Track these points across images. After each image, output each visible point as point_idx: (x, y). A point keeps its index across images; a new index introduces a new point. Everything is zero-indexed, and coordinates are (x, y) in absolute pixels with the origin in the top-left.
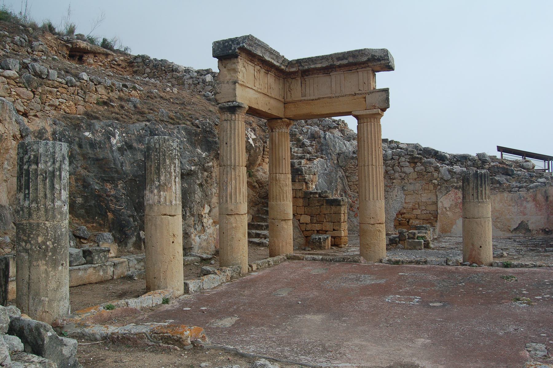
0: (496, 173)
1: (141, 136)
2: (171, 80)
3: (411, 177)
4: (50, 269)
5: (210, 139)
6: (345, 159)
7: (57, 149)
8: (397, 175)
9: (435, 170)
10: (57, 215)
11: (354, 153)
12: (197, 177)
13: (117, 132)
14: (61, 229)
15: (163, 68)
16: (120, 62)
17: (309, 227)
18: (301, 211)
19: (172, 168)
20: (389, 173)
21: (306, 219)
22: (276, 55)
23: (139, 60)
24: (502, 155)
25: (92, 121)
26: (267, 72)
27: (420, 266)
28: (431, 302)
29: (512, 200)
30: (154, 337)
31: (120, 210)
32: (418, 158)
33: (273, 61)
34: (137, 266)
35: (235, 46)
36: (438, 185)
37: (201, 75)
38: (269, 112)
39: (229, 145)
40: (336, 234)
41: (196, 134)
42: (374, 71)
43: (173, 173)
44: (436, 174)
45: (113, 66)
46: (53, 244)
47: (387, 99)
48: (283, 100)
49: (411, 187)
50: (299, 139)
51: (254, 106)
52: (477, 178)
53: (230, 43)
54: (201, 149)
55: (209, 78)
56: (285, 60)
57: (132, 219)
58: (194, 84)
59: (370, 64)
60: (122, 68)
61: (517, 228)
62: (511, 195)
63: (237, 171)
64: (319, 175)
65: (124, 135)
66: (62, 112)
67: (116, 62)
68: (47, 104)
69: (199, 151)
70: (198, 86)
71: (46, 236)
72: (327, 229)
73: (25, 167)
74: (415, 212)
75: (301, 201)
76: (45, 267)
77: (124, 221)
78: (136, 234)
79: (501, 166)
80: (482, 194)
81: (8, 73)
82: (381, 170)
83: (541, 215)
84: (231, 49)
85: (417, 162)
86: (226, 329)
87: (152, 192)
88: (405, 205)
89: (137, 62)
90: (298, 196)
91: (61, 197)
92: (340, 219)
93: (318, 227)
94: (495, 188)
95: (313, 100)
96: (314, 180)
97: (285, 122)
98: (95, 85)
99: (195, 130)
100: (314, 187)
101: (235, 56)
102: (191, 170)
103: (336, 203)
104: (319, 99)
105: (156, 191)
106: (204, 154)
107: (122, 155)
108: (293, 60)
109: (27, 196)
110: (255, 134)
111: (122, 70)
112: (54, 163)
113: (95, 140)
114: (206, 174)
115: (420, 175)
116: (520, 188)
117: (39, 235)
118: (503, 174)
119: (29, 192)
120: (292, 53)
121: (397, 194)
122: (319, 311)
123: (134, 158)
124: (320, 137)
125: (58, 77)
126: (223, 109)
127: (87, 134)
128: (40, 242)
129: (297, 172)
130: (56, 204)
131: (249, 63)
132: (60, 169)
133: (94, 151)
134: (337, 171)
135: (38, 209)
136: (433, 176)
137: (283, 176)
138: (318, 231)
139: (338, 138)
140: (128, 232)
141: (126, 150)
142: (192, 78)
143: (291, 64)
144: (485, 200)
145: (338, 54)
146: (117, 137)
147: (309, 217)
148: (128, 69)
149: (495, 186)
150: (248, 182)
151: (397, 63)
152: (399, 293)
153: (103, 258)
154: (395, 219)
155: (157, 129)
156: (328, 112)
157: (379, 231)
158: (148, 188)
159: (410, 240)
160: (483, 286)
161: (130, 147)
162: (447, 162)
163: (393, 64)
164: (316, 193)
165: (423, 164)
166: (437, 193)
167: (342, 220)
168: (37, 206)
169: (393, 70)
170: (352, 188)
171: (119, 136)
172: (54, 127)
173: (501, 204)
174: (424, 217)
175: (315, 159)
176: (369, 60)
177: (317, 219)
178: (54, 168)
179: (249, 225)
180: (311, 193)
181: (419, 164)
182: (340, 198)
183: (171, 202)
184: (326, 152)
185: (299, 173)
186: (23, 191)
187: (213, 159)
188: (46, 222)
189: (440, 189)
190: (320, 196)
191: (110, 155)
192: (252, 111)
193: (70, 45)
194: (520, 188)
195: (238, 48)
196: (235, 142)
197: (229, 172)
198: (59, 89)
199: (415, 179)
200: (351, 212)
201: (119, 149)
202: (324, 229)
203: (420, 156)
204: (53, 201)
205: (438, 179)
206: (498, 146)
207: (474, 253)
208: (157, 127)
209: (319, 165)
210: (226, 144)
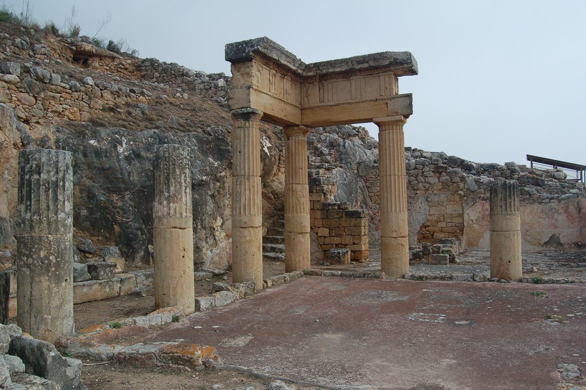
1: (149, 144)
3: (435, 187)
5: (223, 148)
6: (365, 168)
7: (61, 158)
8: (420, 185)
9: (461, 181)
11: (375, 162)
14: (65, 242)
15: (173, 72)
16: (128, 66)
17: (327, 241)
19: (183, 178)
20: (412, 183)
21: (324, 232)
22: (288, 55)
23: (148, 64)
24: (532, 164)
26: (283, 76)
27: (445, 282)
28: (457, 320)
29: (542, 212)
30: (164, 357)
31: (127, 223)
32: (443, 167)
35: (249, 48)
36: (464, 196)
37: (213, 79)
38: (285, 118)
39: (242, 153)
40: (356, 247)
42: (396, 76)
43: (184, 184)
44: (462, 185)
45: (120, 70)
47: (411, 105)
48: (300, 106)
49: (436, 199)
51: (270, 112)
54: (214, 158)
55: (221, 83)
56: (302, 64)
58: (206, 89)
59: (392, 68)
60: (129, 72)
62: (541, 206)
63: (251, 181)
64: (338, 186)
65: (131, 143)
66: (66, 119)
67: (123, 65)
68: (50, 110)
70: (210, 91)
72: (347, 242)
73: (27, 177)
74: (440, 225)
75: (319, 213)
78: (144, 248)
79: (531, 176)
81: (8, 77)
82: (404, 180)
84: (244, 52)
85: (441, 172)
87: (161, 203)
88: (429, 217)
89: (145, 66)
91: (64, 208)
92: (361, 232)
93: (337, 240)
94: (525, 199)
95: (331, 106)
96: (333, 191)
97: (302, 129)
98: (101, 90)
100: (333, 198)
102: (202, 181)
103: (356, 215)
104: (338, 105)
105: (165, 203)
106: (216, 164)
107: (130, 164)
108: (311, 64)
109: (29, 208)
111: (130, 74)
112: (57, 173)
113: (101, 148)
114: (218, 184)
115: (445, 186)
116: (551, 199)
117: (41, 249)
119: (31, 203)
121: (421, 206)
122: (338, 330)
123: (142, 168)
124: (339, 145)
126: (236, 116)
127: (92, 142)
128: (42, 256)
129: (315, 182)
130: (60, 216)
131: (264, 67)
132: (63, 179)
133: (99, 160)
134: (357, 181)
135: (41, 221)
136: (458, 186)
137: (299, 187)
139: (358, 146)
140: (136, 246)
141: (133, 159)
142: (203, 82)
143: (308, 67)
145: (358, 57)
146: (124, 146)
148: (135, 73)
149: (525, 197)
152: (423, 311)
154: (419, 232)
155: (166, 137)
157: (402, 245)
159: (435, 255)
161: (138, 156)
162: (474, 172)
163: (417, 68)
164: (335, 205)
165: (448, 174)
166: (464, 205)
167: (363, 233)
168: (40, 219)
169: (417, 74)
170: (373, 199)
171: (126, 144)
172: (58, 134)
173: (531, 217)
174: (450, 230)
175: (334, 168)
176: (391, 64)
177: (336, 232)
178: (57, 178)
179: (264, 238)
180: (330, 205)
181: (444, 174)
182: (360, 210)
183: (181, 214)
184: (346, 161)
185: (317, 183)
186: (24, 202)
187: (225, 169)
188: (49, 236)
189: (466, 200)
190: (339, 208)
191: (117, 164)
192: (267, 118)
193: (74, 48)
194: (551, 199)
195: (252, 51)
196: (249, 150)
197: (243, 182)
198: (63, 94)
199: (440, 190)
200: (372, 225)
201: (127, 158)
203: (445, 165)
204: (56, 213)
205: (464, 190)
206: (527, 155)
209: (338, 175)
210: (240, 152)
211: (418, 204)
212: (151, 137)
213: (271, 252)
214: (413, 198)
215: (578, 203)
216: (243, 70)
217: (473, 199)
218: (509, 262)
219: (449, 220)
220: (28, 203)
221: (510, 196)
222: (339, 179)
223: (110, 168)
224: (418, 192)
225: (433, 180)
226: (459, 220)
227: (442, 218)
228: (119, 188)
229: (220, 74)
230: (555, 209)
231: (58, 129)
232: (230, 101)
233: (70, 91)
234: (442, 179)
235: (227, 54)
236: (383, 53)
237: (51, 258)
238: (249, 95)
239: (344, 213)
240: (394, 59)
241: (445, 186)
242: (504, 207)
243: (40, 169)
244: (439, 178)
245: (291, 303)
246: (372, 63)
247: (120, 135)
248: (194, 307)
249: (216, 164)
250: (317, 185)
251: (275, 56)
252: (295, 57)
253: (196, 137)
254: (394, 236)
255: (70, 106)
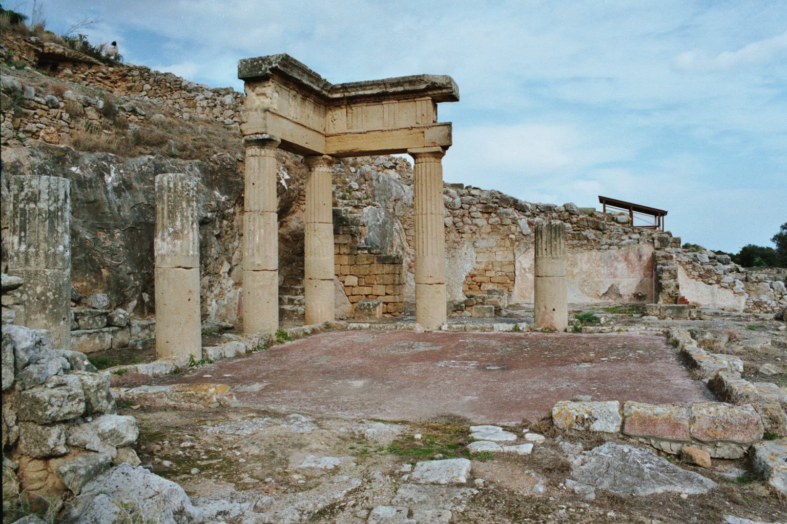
0: (585, 228)
1: (143, 174)
2: (178, 101)
3: (483, 231)
4: (51, 324)
5: (231, 179)
6: (403, 207)
8: (466, 228)
9: (513, 223)
10: (58, 261)
12: (215, 226)
13: (113, 168)
14: (63, 278)
15: (168, 85)
16: (109, 75)
17: (356, 291)
18: (346, 270)
21: (353, 280)
22: (316, 78)
24: (604, 207)
25: (81, 153)
27: (485, 333)
28: (489, 366)
29: (601, 259)
30: (175, 396)
31: (118, 266)
32: (492, 207)
33: (312, 85)
34: (140, 334)
35: (266, 66)
36: (516, 240)
37: (219, 95)
38: (306, 146)
41: (213, 172)
43: (190, 218)
44: (513, 228)
45: (99, 79)
46: (54, 295)
50: (345, 180)
52: (551, 229)
53: (260, 62)
55: (228, 99)
56: (327, 84)
57: (132, 278)
60: (112, 82)
61: (606, 293)
62: (599, 253)
65: (121, 171)
66: (40, 140)
67: (104, 74)
68: (21, 129)
69: (217, 193)
70: (215, 110)
71: (45, 285)
73: (21, 206)
74: (488, 274)
75: (346, 258)
76: (45, 321)
77: (122, 279)
78: (137, 296)
79: (591, 219)
80: (556, 248)
83: (633, 277)
84: (260, 69)
85: (491, 213)
86: (255, 393)
88: (476, 266)
89: (132, 76)
90: (342, 252)
93: (367, 290)
94: (582, 245)
95: (361, 133)
97: (326, 159)
99: (212, 167)
100: (363, 241)
101: (264, 79)
102: (206, 217)
104: (368, 132)
106: (224, 198)
107: (119, 196)
109: (23, 239)
110: (288, 174)
111: (112, 85)
113: (84, 177)
114: (225, 222)
115: (494, 228)
116: (610, 245)
117: (37, 285)
118: (593, 229)
119: (25, 235)
120: (335, 77)
122: (361, 376)
123: (134, 201)
124: (372, 180)
125: (36, 95)
127: (74, 169)
128: (38, 292)
129: (341, 222)
131: (283, 87)
133: (83, 191)
135: (37, 254)
136: (510, 229)
138: (366, 296)
139: (395, 181)
140: (128, 293)
141: (124, 191)
144: (559, 256)
145: (392, 79)
146: (113, 174)
147: (357, 278)
148: (119, 84)
150: (279, 233)
151: (462, 93)
152: (455, 359)
153: (100, 323)
154: (464, 283)
155: (163, 165)
156: (379, 149)
158: (160, 235)
159: (478, 306)
160: (550, 350)
162: (528, 213)
163: (458, 94)
164: (365, 248)
165: (498, 215)
166: (515, 251)
168: (36, 252)
171: (115, 173)
172: (32, 159)
173: (589, 265)
174: (499, 280)
176: (428, 89)
177: (366, 280)
179: (280, 288)
180: (359, 249)
181: (493, 215)
186: (17, 233)
188: (46, 270)
189: (518, 246)
191: (104, 196)
192: (286, 146)
193: (40, 49)
194: (610, 245)
195: (270, 69)
198: (38, 111)
199: (489, 233)
201: (115, 189)
202: (374, 293)
205: (517, 234)
206: (600, 197)
207: (546, 316)
208: (164, 162)
209: (370, 215)
211: (464, 250)
212: (145, 164)
213: (289, 304)
214: (457, 242)
215: (638, 250)
216: (259, 89)
217: (526, 244)
218: (554, 310)
219: (499, 269)
220: (23, 234)
221: (555, 238)
222: (371, 219)
223: (95, 201)
224: (463, 235)
225: (481, 222)
226: (511, 268)
227: (490, 266)
228: (107, 225)
229: (227, 89)
230: (614, 256)
231: (32, 152)
232: (243, 125)
233: (46, 107)
234: (491, 221)
235: (240, 71)
236: (420, 76)
237: (48, 294)
238: (264, 119)
239: (375, 258)
240: (432, 83)
241: (494, 228)
242: (549, 250)
243: (36, 198)
244: (487, 219)
245: (312, 355)
246: (408, 87)
247: (107, 161)
248: (277, 243)
249: (223, 199)
250: (344, 225)
251: (296, 76)
252: (319, 76)
253: (199, 166)
254: (429, 282)
255: (46, 125)
